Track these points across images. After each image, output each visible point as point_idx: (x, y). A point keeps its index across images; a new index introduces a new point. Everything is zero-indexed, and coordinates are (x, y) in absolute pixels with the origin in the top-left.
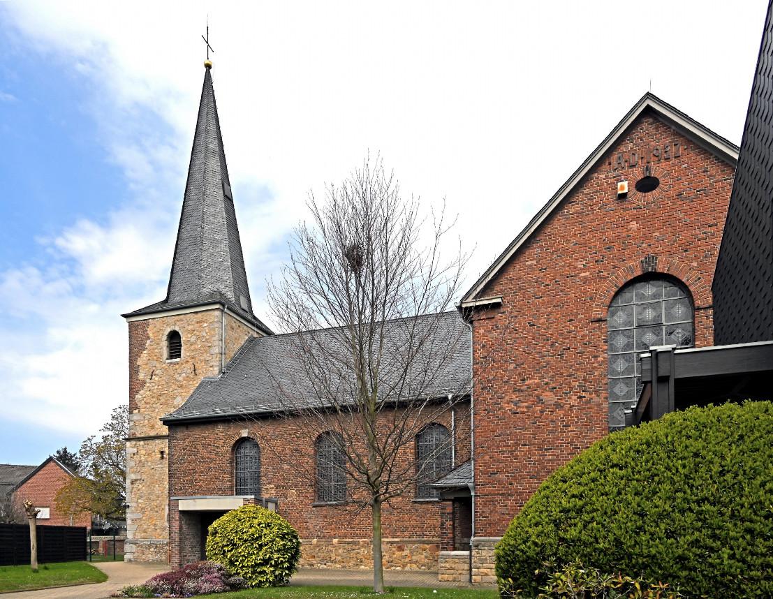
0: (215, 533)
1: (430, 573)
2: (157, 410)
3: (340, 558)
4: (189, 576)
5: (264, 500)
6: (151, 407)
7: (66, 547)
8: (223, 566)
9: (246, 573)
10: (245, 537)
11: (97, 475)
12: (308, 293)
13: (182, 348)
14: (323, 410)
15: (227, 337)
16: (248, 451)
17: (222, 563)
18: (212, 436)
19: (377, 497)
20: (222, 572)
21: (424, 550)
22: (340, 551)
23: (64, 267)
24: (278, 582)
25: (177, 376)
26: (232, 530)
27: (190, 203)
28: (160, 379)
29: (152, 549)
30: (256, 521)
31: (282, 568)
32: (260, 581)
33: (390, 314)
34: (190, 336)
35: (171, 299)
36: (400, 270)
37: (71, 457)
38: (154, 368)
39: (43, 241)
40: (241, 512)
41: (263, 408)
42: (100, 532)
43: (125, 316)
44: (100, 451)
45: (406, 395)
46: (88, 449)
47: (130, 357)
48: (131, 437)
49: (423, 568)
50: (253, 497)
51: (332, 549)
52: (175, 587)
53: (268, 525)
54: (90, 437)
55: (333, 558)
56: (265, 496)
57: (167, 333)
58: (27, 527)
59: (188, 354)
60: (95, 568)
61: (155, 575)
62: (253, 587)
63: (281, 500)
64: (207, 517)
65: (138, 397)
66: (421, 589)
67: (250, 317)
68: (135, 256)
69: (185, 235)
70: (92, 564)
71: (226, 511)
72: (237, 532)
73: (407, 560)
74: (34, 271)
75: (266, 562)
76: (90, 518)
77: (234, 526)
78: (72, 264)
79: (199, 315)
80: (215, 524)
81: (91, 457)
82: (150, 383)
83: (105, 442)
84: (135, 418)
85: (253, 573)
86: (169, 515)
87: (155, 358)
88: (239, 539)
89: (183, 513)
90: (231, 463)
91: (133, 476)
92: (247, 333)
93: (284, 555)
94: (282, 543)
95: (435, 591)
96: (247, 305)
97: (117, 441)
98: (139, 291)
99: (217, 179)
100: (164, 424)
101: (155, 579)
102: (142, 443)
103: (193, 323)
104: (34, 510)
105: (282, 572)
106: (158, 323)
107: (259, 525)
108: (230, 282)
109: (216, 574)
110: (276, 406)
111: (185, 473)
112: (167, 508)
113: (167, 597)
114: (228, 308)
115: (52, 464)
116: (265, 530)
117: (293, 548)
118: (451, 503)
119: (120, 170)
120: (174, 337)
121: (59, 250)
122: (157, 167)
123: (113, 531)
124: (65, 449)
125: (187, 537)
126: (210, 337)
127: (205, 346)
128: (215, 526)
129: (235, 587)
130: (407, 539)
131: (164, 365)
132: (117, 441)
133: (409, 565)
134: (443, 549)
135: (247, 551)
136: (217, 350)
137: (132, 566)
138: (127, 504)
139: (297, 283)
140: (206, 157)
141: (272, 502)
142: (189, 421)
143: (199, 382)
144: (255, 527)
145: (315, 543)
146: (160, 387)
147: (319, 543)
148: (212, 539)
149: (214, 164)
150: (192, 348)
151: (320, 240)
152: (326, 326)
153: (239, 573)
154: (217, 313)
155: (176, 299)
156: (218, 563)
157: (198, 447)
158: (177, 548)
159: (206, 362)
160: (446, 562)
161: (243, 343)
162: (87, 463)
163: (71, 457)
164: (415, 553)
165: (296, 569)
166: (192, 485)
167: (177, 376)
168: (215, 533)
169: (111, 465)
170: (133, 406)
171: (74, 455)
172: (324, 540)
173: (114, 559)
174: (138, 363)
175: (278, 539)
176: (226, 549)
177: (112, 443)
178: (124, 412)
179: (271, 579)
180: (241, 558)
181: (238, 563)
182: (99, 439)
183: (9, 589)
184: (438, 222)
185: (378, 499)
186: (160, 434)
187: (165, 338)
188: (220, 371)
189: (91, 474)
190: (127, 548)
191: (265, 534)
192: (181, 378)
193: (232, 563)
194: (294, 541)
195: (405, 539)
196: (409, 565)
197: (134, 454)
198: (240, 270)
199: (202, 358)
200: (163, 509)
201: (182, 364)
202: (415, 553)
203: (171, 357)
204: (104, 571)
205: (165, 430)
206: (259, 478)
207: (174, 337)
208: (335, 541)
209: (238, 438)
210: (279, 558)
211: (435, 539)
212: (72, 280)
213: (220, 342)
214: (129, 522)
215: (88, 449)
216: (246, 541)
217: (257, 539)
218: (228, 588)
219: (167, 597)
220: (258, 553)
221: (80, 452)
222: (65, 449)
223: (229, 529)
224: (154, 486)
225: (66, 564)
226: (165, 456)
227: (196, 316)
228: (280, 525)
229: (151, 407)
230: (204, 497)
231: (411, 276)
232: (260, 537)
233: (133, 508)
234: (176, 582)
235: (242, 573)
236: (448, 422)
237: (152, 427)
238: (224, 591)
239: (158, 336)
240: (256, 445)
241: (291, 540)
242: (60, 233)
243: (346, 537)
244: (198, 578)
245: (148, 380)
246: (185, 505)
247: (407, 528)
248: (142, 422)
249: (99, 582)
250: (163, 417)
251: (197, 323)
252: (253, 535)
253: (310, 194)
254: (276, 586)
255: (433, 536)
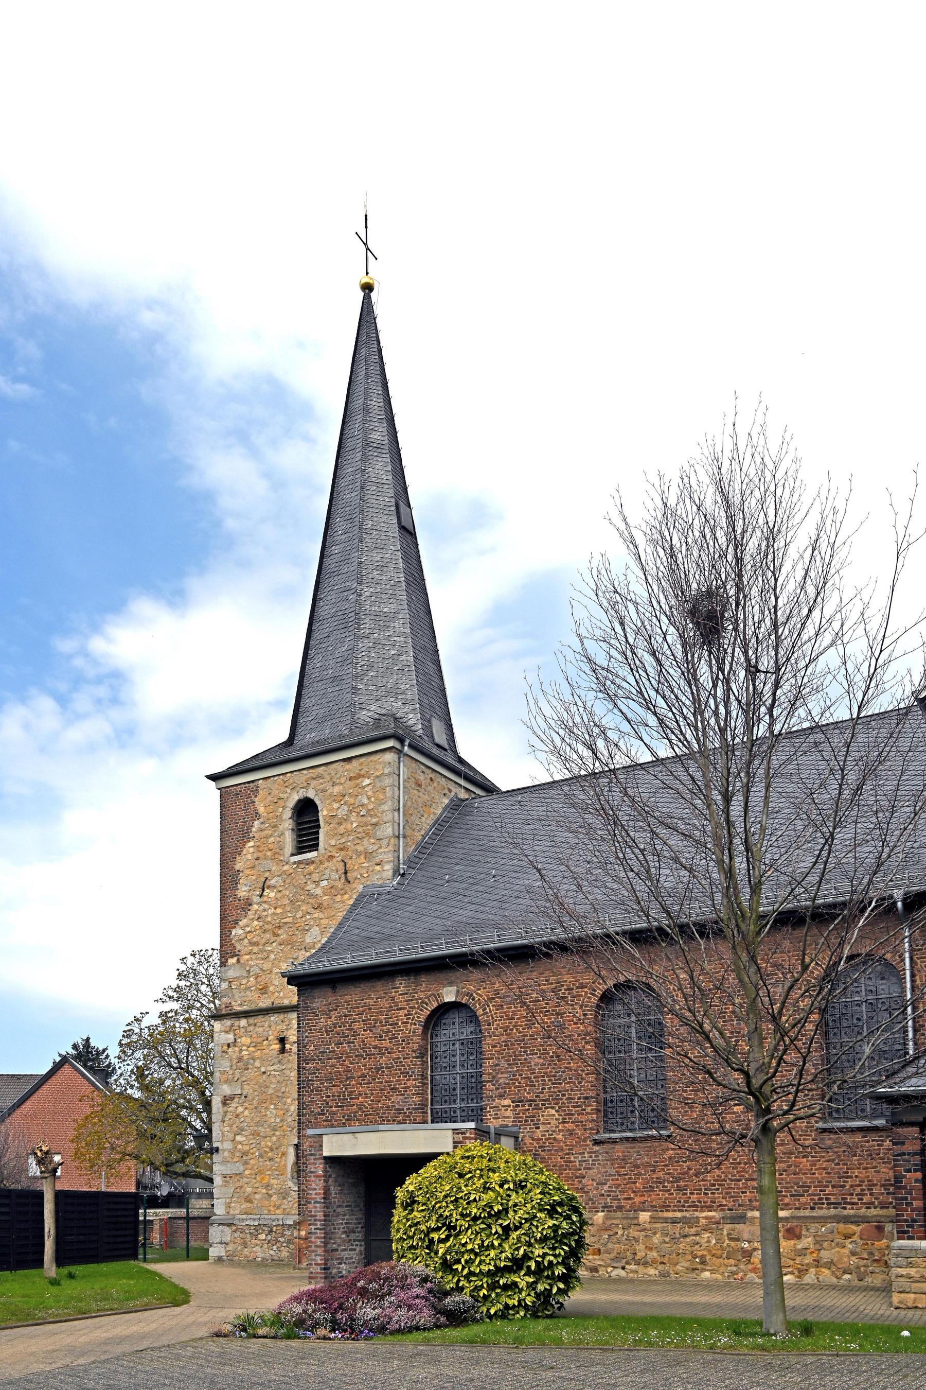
0: (410, 1204)
1: (867, 1289)
2: (272, 956)
3: (655, 1254)
4: (363, 1293)
5: (492, 1131)
6: (261, 951)
7: (104, 1231)
8: (429, 1271)
9: (478, 1288)
10: (475, 1210)
11: (144, 1088)
12: (612, 698)
13: (321, 832)
14: (637, 937)
15: (409, 803)
16: (456, 1029)
17: (427, 1266)
18: (384, 1003)
19: (767, 1121)
20: (429, 1285)
21: (847, 1237)
22: (656, 1239)
23: (102, 691)
24: (544, 1308)
25: (311, 886)
26: (446, 1196)
27: (335, 549)
28: (279, 895)
29: (263, 1236)
30: (495, 1177)
31: (552, 1277)
32: (507, 1307)
33: (800, 720)
34: (336, 806)
35: (390, 732)
36: (810, 630)
37: (98, 1054)
38: (267, 874)
39: (66, 645)
40: (463, 1158)
41: (512, 939)
42: (154, 1202)
43: (214, 778)
44: (151, 1042)
45: (828, 896)
46: (135, 1038)
47: (222, 855)
48: (224, 1012)
49: (847, 1276)
50: (472, 1125)
51: (636, 1234)
52: (339, 1316)
53: (520, 1186)
54: (139, 1016)
55: (640, 1255)
56: (493, 1124)
57: (292, 803)
58: (40, 1195)
59: (333, 843)
60: (156, 1274)
61: (296, 1291)
62: (490, 1317)
63: (524, 1134)
64: (391, 1170)
65: (237, 932)
66: (872, 1328)
67: (451, 761)
68: (225, 659)
69: (324, 610)
70: (163, 1268)
71: (435, 1156)
72: (456, 1200)
73: (808, 1259)
74: (47, 704)
75: (517, 1264)
76: (133, 1172)
77: (452, 1188)
78: (114, 684)
79: (355, 763)
80: (411, 1183)
81: (138, 1054)
82: (260, 904)
83: (164, 1023)
84: (231, 973)
85: (492, 1287)
86: (297, 1163)
87: (269, 853)
88: (462, 1215)
89: (333, 1161)
90: (422, 1055)
91: (226, 1090)
92: (446, 791)
93: (554, 1249)
94: (551, 1223)
95: (906, 1333)
96: (445, 736)
97: (187, 1020)
98: (232, 725)
99: (388, 496)
100: (289, 983)
101: (297, 1299)
102: (243, 1022)
103: (342, 781)
104: (51, 1161)
105: (551, 1286)
106: (275, 786)
107: (501, 1186)
108: (413, 694)
109: (417, 1291)
110: (542, 931)
111: (329, 1080)
112: (291, 1151)
113: (325, 1338)
114: (410, 746)
115: (67, 1069)
116: (514, 1195)
117: (572, 1234)
118: (917, 1129)
119: (206, 498)
120: (306, 811)
121: (95, 662)
122: (277, 482)
123: (176, 1199)
124: (88, 1039)
125: (339, 1210)
126: (376, 804)
127: (366, 824)
128: (411, 1188)
129: (456, 1318)
130: (807, 1213)
131: (286, 867)
132: (187, 1020)
133: (812, 1270)
134: (902, 1234)
135: (478, 1242)
136: (388, 830)
137: (225, 1271)
138: (215, 1145)
139: (587, 681)
140: (364, 458)
141: (508, 1135)
142: (356, 973)
143: (355, 896)
144: (493, 1190)
145: (601, 1221)
146: (279, 911)
147: (609, 1222)
148: (405, 1217)
149: (380, 469)
150: (341, 829)
151: (639, 590)
152: (646, 757)
153: (462, 1289)
154: (390, 757)
155: (307, 737)
156: (419, 1267)
157: (356, 1026)
158: (320, 1234)
159: (368, 855)
160: (910, 1265)
161: (439, 812)
162: (125, 1069)
163: (98, 1054)
164: (826, 1244)
165: (578, 1279)
166: (343, 1100)
167: (311, 886)
168: (410, 1204)
169: (175, 1068)
170: (227, 950)
171: (104, 1050)
172: (619, 1214)
173: (188, 1257)
174: (237, 867)
175: (543, 1216)
176: (435, 1236)
177: (177, 1025)
178: (200, 963)
179: (529, 1301)
180: (466, 1257)
181: (460, 1267)
182: (153, 1019)
183: (20, 1320)
184: (902, 521)
185: (769, 1125)
186: (278, 1003)
187: (288, 813)
188: (396, 872)
189: (132, 1087)
190: (215, 1233)
191: (515, 1205)
192: (318, 891)
193: (447, 1266)
194: (574, 1218)
195: (802, 1213)
196: (812, 1270)
197: (229, 1046)
198: (432, 667)
199: (360, 848)
200: (283, 1154)
201: (321, 862)
202: (826, 1244)
203: (301, 848)
204: (176, 1281)
205: (290, 995)
206: (480, 1084)
207: (306, 811)
208: (644, 1216)
209: (435, 1005)
210: (545, 1254)
211: (873, 1212)
212: (115, 714)
213: (396, 814)
214: (218, 1180)
215: (135, 1038)
216: (475, 1219)
217: (498, 1215)
218: (443, 1319)
219: (325, 1338)
220: (500, 1245)
221: (121, 1045)
222: (88, 1039)
223: (441, 1195)
224: (267, 1108)
225: (104, 1267)
226: (287, 1046)
227: (348, 766)
228: (545, 1184)
229: (261, 951)
230: (375, 1127)
231: (838, 637)
232: (506, 1210)
233: (226, 1154)
234: (340, 1307)
235: (469, 1287)
236: (895, 951)
237: (264, 990)
238: (438, 1326)
239: (276, 811)
240: (473, 1018)
241: (568, 1217)
242: (96, 628)
243: (667, 1208)
244: (382, 1297)
245: (256, 899)
246: (338, 1144)
247: (806, 1187)
248: (244, 982)
249: (177, 1305)
250: (285, 967)
251: (351, 779)
252: (491, 1207)
253: (617, 498)
254: (538, 1317)
255: (869, 1205)
